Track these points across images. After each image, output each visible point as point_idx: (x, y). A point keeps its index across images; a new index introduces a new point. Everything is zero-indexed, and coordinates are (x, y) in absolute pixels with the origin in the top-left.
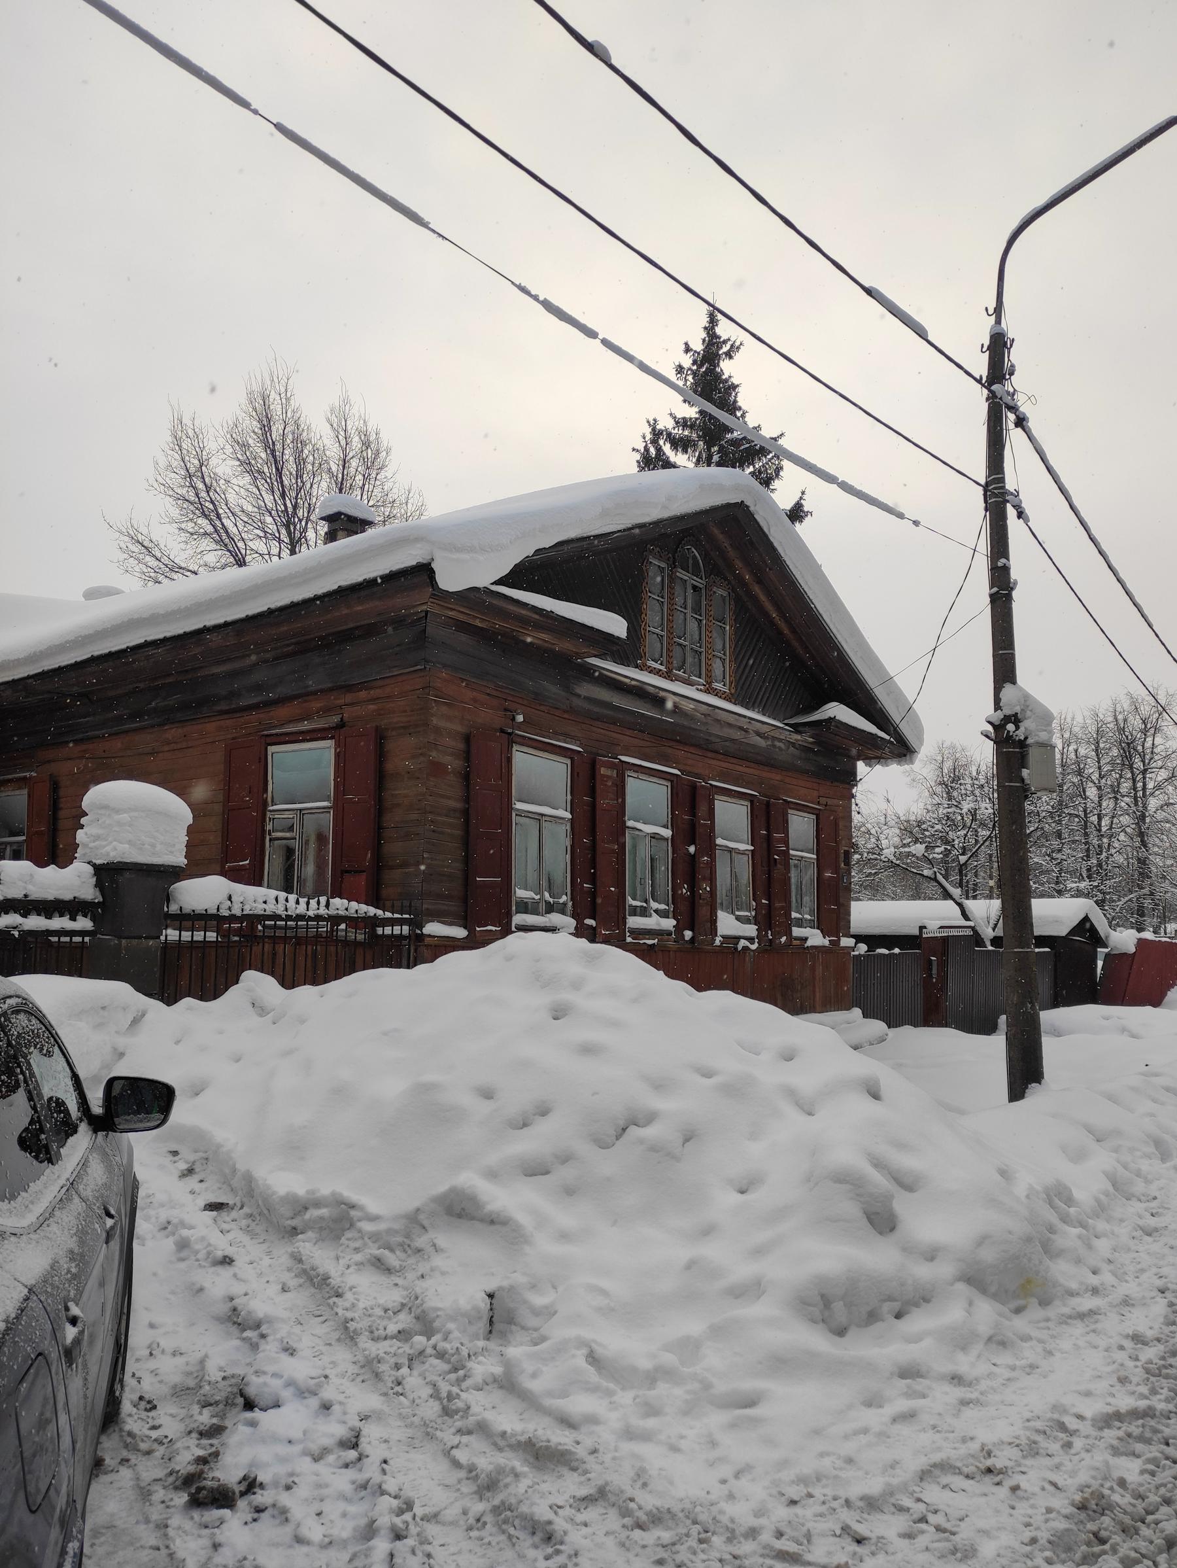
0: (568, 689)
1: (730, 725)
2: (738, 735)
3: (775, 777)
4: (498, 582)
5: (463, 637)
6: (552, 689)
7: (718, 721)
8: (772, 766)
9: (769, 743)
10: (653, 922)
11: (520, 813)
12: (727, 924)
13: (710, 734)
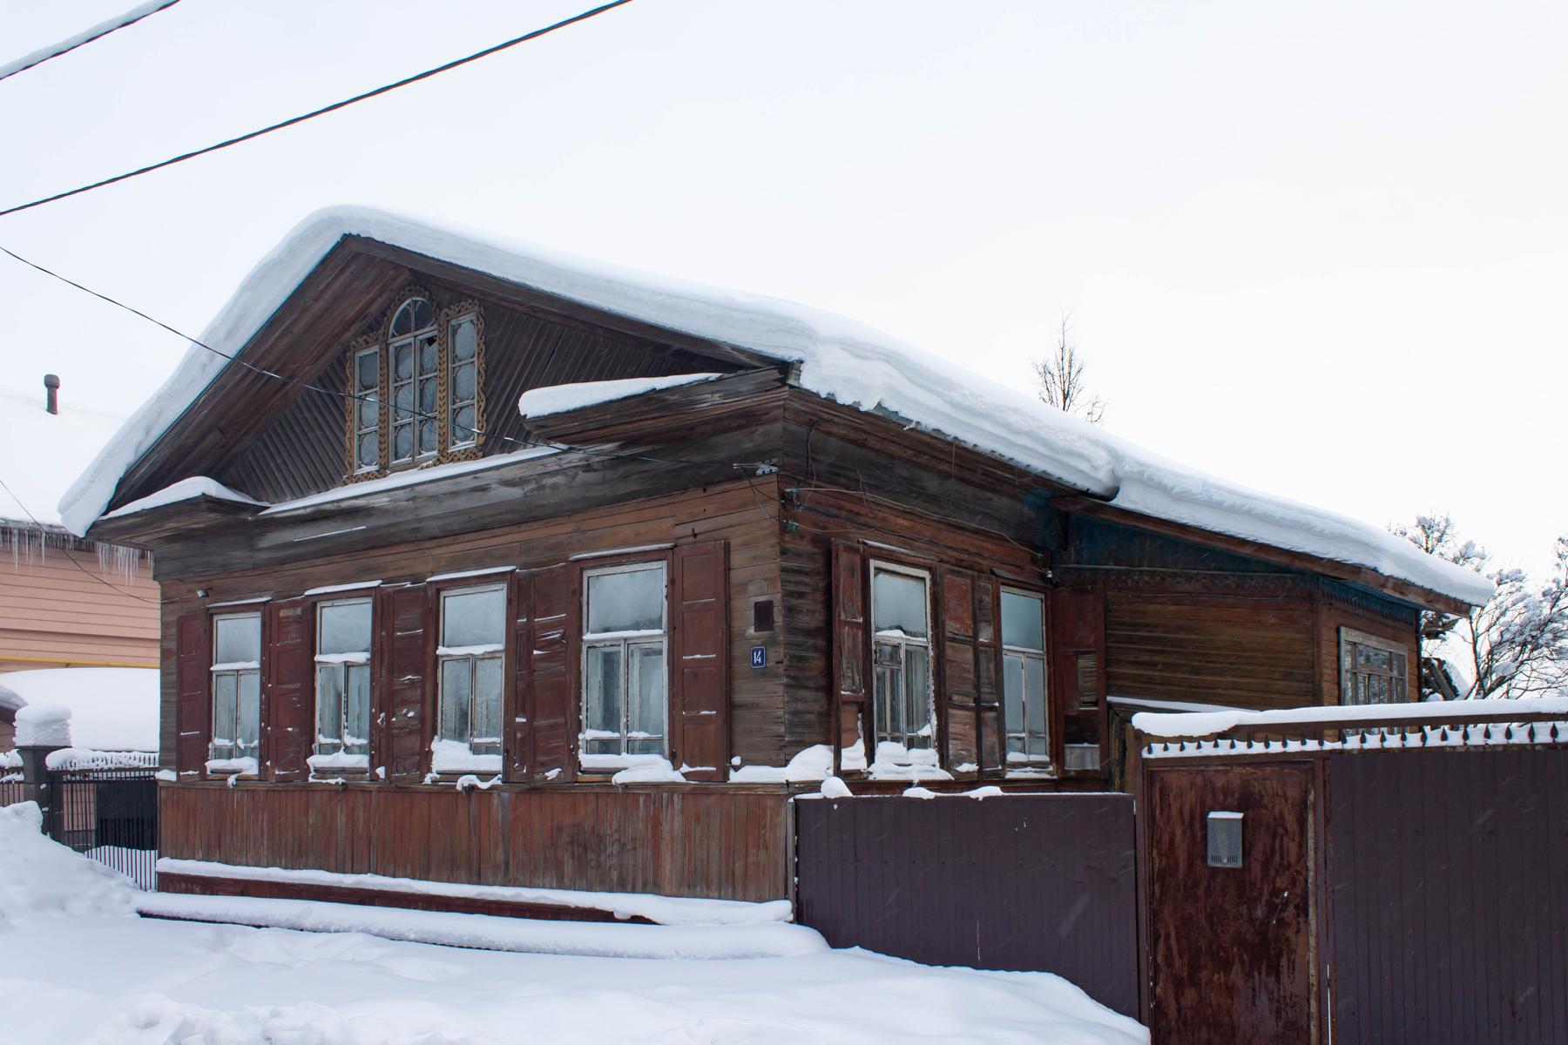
0: (252, 548)
1: (454, 494)
2: (476, 501)
3: (560, 531)
4: (114, 504)
5: (177, 546)
6: (239, 555)
7: (432, 497)
8: (536, 519)
9: (533, 486)
10: (342, 760)
11: (221, 674)
12: (448, 755)
13: (420, 520)
